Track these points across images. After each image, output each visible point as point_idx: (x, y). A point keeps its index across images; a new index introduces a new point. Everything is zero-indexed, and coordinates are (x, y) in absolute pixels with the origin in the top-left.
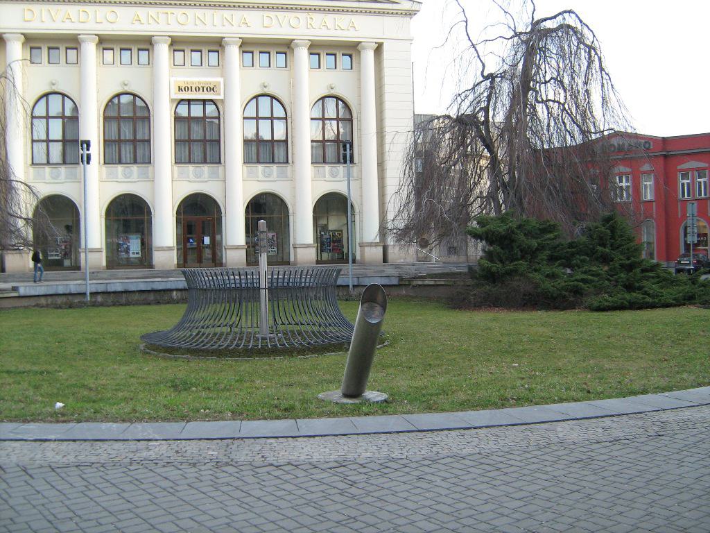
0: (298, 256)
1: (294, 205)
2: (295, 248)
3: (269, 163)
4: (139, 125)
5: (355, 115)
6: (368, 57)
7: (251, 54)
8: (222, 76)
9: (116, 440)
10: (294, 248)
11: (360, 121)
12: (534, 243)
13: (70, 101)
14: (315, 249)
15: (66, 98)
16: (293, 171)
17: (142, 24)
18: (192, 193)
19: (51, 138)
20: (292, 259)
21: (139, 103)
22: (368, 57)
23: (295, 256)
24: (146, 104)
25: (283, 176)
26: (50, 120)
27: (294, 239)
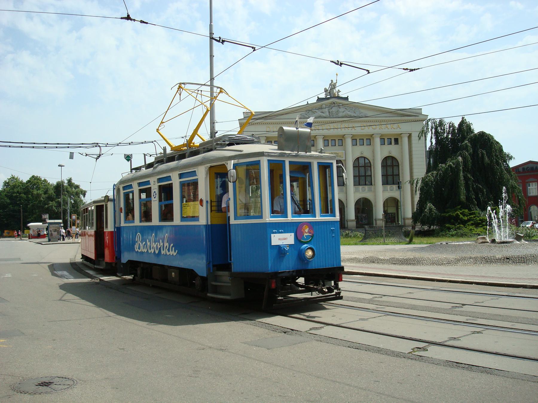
0: (378, 224)
1: (375, 202)
2: (347, 221)
3: (364, 185)
4: (395, 168)
5: (400, 163)
6: (405, 140)
7: (369, 140)
8: (344, 150)
9: (387, 306)
10: (404, 220)
11: (402, 166)
12: (466, 218)
13: (367, 160)
14: (355, 222)
15: (366, 159)
16: (375, 188)
17: (388, 129)
18: (395, 197)
19: (360, 175)
20: (346, 226)
21: (367, 161)
22: (405, 140)
23: (376, 224)
24: (369, 161)
25: (370, 190)
26: (388, 167)
27: (347, 218)
